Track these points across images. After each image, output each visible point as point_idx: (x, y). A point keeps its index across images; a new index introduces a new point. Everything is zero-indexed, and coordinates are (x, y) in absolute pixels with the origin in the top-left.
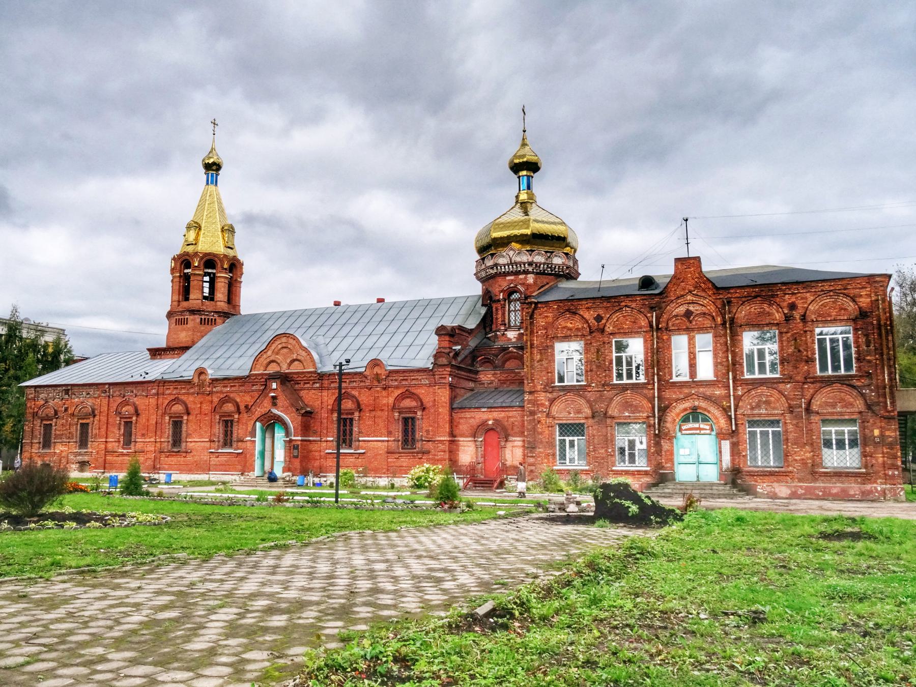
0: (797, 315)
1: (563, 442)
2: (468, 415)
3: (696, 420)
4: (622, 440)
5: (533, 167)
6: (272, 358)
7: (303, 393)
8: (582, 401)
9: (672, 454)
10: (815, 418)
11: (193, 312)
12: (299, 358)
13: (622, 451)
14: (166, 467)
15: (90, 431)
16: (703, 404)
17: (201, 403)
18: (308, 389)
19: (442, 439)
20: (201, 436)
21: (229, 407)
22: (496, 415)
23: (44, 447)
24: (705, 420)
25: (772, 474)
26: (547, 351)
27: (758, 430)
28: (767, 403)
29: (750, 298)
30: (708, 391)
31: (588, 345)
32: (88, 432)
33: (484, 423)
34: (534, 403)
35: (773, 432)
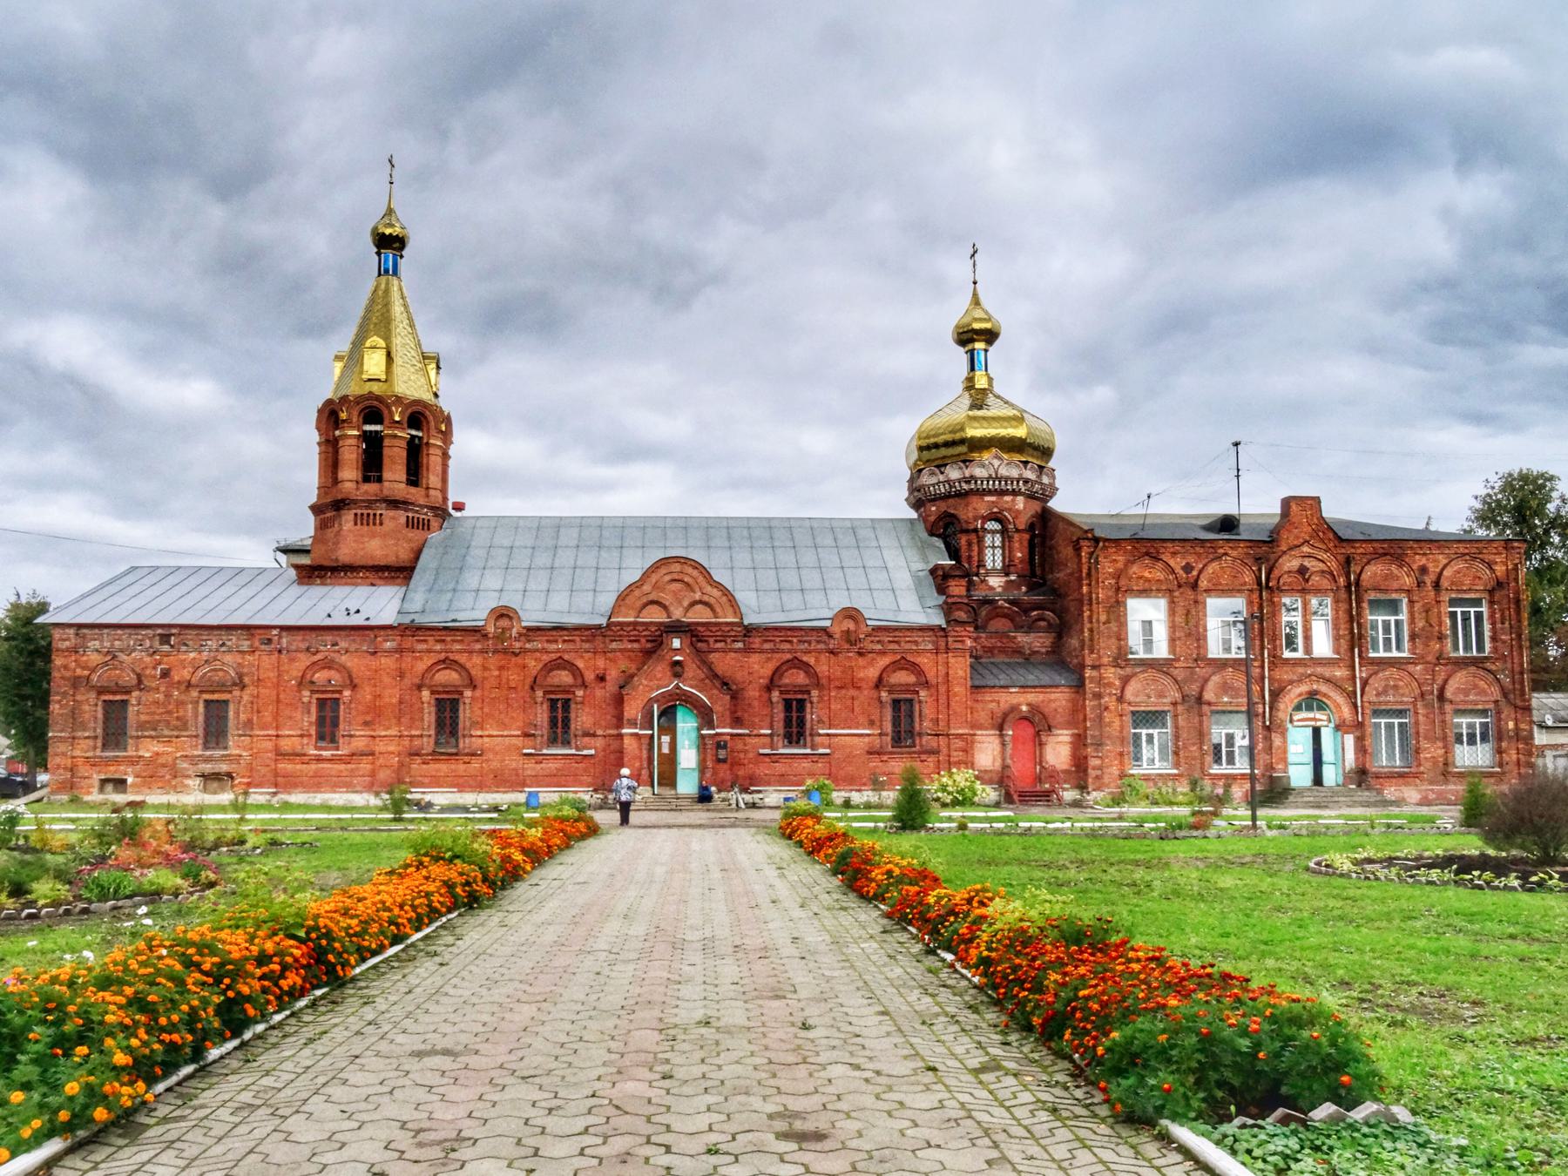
0: (1429, 580)
1: (1137, 737)
2: (988, 697)
3: (1309, 708)
4: (1218, 733)
5: (990, 336)
6: (651, 597)
7: (713, 657)
8: (1167, 681)
9: (1285, 752)
10: (1205, 708)
11: (394, 504)
12: (706, 598)
13: (1217, 748)
14: (426, 780)
15: (231, 714)
16: (1324, 688)
17: (501, 668)
18: (724, 651)
20: (504, 726)
21: (564, 677)
22: (1033, 697)
23: (105, 746)
24: (1320, 708)
25: (1402, 776)
26: (1117, 610)
27: (1383, 721)
28: (1396, 687)
29: (1378, 556)
30: (1327, 672)
31: (1172, 604)
32: (226, 718)
33: (1014, 709)
34: (1099, 681)
35: (1400, 725)
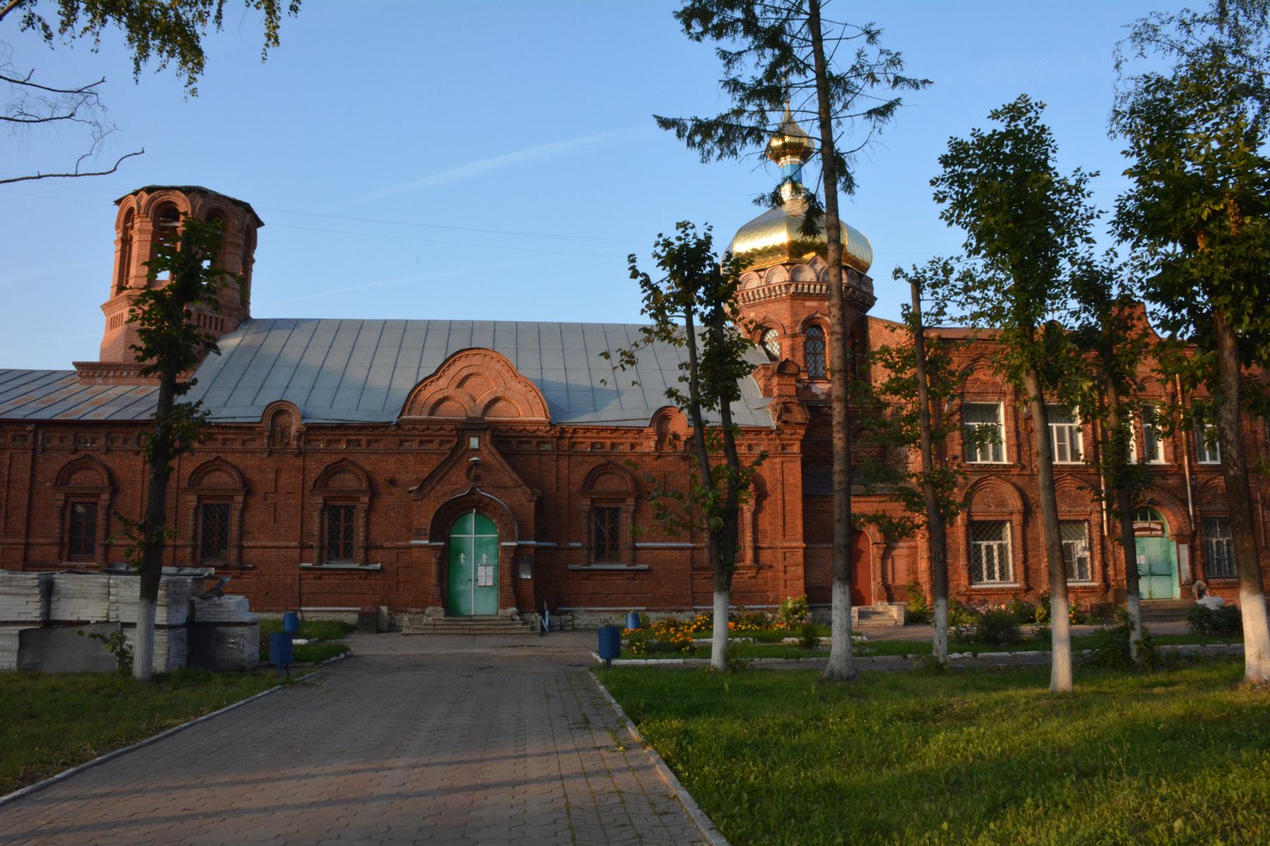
19: (792, 544)
